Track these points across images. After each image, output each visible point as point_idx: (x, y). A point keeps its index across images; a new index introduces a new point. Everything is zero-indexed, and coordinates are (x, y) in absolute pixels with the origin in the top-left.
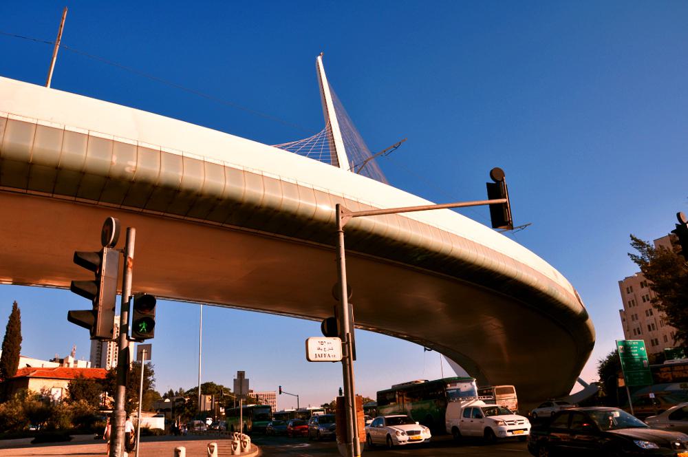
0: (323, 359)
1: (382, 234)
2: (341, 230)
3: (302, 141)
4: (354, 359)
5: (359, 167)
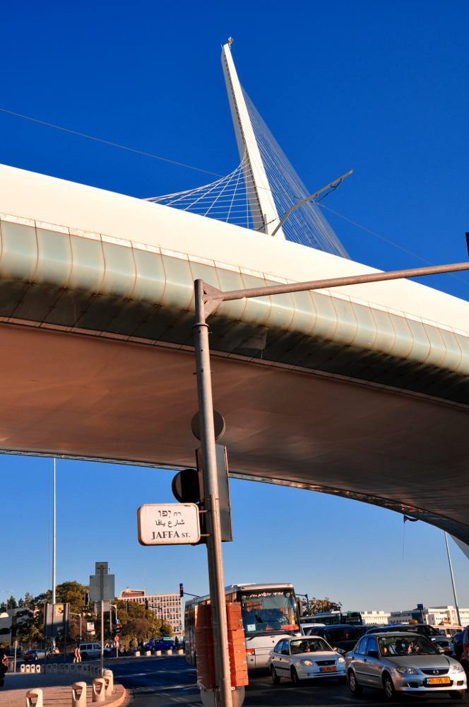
0: (167, 540)
1: (308, 330)
2: (203, 322)
3: (200, 189)
4: (227, 537)
5: (296, 231)
